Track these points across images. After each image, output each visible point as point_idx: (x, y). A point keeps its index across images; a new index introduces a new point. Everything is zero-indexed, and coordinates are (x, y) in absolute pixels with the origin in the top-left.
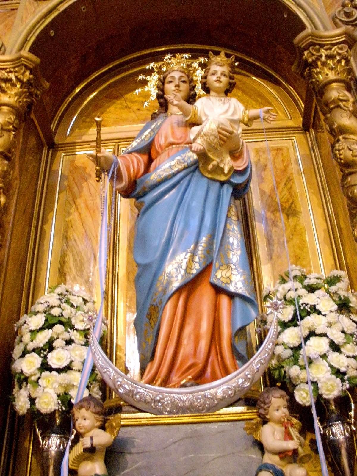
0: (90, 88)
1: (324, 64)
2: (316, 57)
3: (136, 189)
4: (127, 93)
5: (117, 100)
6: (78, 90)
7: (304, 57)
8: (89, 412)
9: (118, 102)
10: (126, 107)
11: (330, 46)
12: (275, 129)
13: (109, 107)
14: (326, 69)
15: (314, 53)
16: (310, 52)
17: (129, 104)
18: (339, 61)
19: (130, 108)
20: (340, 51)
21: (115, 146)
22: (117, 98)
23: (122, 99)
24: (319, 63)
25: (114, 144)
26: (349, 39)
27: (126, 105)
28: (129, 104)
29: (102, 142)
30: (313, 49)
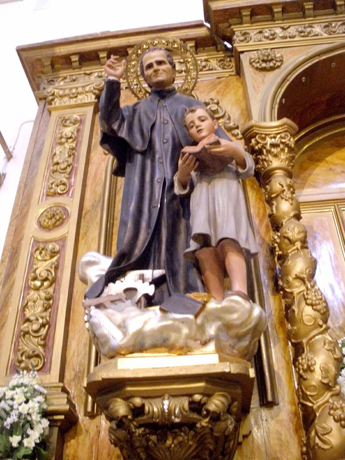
0: (169, 154)
1: (269, 152)
2: (261, 145)
3: (131, 259)
4: (327, 157)
5: (320, 163)
6: (305, 148)
7: (251, 144)
8: (109, 424)
9: (321, 164)
10: (331, 169)
11: (274, 135)
12: (319, 201)
13: (314, 169)
14: (270, 156)
15: (260, 141)
16: (256, 140)
17: (333, 167)
18: (283, 150)
19: (334, 170)
20: (283, 140)
21: (334, 206)
22: (319, 160)
23: (324, 162)
24: (264, 151)
25: (334, 204)
26: (289, 129)
27: (330, 167)
28: (333, 167)
29: (301, 204)
30: (259, 137)
